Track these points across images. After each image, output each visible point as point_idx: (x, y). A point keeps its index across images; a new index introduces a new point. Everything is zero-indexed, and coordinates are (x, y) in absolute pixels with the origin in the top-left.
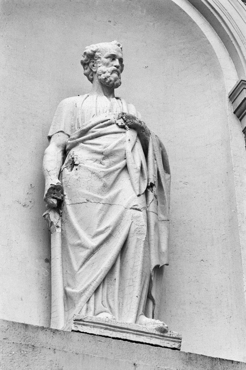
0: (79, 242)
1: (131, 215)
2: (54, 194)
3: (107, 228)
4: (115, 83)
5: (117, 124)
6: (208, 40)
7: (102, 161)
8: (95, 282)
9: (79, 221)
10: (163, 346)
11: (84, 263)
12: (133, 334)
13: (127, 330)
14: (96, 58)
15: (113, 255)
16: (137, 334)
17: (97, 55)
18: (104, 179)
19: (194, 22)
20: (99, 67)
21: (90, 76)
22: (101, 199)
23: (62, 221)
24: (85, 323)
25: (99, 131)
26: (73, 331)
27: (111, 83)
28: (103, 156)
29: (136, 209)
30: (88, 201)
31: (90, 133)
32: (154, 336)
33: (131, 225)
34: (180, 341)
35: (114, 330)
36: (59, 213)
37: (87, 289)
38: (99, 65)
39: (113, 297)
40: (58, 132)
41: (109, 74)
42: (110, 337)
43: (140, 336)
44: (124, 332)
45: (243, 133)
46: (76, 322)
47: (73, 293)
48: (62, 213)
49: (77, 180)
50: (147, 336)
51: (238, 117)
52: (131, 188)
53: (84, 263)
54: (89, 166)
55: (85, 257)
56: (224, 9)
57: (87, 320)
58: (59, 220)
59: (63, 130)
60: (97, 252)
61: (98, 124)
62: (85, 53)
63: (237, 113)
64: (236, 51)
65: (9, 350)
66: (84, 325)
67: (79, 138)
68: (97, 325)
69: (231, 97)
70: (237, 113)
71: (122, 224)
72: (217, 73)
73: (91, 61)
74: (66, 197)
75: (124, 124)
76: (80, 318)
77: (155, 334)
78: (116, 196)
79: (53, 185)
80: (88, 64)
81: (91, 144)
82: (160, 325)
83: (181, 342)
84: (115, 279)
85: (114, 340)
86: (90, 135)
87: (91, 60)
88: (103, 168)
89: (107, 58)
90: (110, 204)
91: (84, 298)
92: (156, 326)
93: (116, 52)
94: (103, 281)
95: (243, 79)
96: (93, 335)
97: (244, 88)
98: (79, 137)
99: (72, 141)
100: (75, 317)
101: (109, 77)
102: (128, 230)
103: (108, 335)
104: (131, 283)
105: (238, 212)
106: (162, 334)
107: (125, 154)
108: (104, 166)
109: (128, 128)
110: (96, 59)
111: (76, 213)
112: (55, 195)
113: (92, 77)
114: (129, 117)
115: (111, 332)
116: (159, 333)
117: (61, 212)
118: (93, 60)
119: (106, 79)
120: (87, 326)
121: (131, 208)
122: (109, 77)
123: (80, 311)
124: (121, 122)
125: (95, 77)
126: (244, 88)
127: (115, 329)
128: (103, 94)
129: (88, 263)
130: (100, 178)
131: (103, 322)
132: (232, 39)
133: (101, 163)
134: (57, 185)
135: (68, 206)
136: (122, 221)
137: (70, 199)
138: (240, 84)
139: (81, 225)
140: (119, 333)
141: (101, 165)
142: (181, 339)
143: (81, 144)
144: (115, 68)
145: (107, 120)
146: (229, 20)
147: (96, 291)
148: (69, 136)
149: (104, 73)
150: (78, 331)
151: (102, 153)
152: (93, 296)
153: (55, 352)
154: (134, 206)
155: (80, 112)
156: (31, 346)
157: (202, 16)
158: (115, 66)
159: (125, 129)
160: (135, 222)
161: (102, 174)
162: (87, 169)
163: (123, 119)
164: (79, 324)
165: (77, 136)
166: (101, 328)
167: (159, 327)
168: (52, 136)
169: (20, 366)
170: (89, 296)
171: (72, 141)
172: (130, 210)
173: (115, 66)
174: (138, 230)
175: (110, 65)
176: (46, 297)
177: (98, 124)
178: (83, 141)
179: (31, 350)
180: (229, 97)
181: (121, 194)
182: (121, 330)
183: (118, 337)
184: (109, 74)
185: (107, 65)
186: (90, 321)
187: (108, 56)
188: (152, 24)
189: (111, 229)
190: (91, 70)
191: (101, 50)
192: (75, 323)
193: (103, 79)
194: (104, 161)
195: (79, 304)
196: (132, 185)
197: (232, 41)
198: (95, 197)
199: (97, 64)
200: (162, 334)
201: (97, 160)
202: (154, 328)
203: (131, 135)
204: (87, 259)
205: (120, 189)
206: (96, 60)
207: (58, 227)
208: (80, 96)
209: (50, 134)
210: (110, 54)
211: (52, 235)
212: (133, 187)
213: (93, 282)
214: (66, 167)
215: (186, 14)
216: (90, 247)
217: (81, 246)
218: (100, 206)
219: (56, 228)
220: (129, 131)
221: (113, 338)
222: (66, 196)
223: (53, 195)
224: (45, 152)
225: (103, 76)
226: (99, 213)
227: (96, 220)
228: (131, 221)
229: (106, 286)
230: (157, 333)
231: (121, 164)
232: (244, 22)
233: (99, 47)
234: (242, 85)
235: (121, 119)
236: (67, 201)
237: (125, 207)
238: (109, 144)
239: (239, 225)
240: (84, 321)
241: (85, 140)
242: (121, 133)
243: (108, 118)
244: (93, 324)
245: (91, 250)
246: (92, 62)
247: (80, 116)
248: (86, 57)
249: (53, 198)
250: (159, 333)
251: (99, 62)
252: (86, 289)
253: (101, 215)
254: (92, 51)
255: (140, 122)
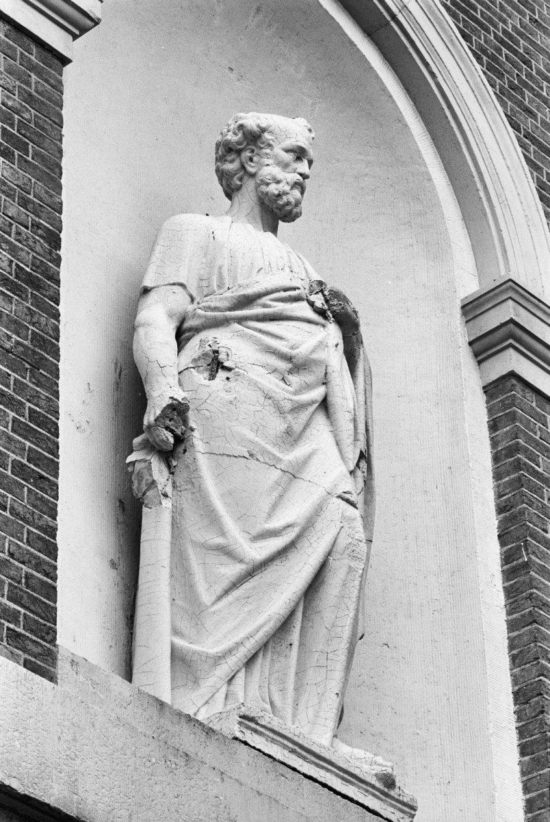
0: (219, 540)
1: (340, 511)
2: (170, 421)
3: (289, 526)
4: (295, 210)
5: (312, 304)
6: (428, 173)
7: (286, 375)
8: (252, 641)
9: (222, 496)
10: (385, 816)
11: (226, 592)
12: (337, 775)
13: (329, 764)
14: (263, 143)
15: (295, 589)
16: (343, 779)
17: (267, 139)
18: (289, 417)
19: (406, 126)
20: (268, 165)
21: (235, 178)
22: (279, 460)
23: (174, 486)
24: (258, 728)
25: (280, 308)
26: (236, 739)
27: (288, 208)
28: (290, 366)
29: (348, 501)
30: (251, 455)
31: (257, 305)
32: (371, 790)
33: (339, 533)
34: (413, 812)
35: (305, 758)
36: (169, 466)
37: (234, 652)
38: (267, 161)
39: (283, 682)
40: (174, 284)
41: (287, 188)
42: (299, 772)
43: (347, 784)
44: (323, 768)
45: (482, 391)
46: (243, 720)
47: (200, 654)
48: (175, 467)
49: (231, 402)
50: (359, 787)
51: (476, 355)
52: (336, 451)
53: (226, 592)
54: (259, 380)
55: (233, 579)
56: (471, 117)
57: (263, 723)
58: (167, 480)
59: (185, 283)
60: (260, 576)
61: (277, 290)
62: (241, 127)
63: (477, 346)
64: (485, 215)
65: (145, 751)
66: (256, 731)
67: (230, 311)
68: (278, 738)
69: (467, 308)
70: (477, 346)
71: (318, 526)
72: (438, 250)
73: (250, 147)
74: (196, 434)
75: (326, 307)
76: (252, 715)
77: (373, 787)
78: (309, 457)
79: (176, 400)
80: (239, 152)
81: (260, 331)
82: (386, 768)
83: (413, 816)
84: (291, 645)
85: (306, 781)
86: (256, 310)
87: (248, 144)
88: (287, 391)
89: (287, 151)
90: (293, 474)
91: (224, 669)
92: (378, 769)
93: (307, 143)
94: (264, 646)
95: (512, 278)
96: (272, 760)
97: (511, 298)
98: (230, 309)
99: (210, 314)
100: (243, 710)
101: (288, 194)
102: (332, 541)
103: (296, 767)
104: (323, 662)
105: (478, 559)
106: (386, 790)
107: (326, 373)
108: (290, 388)
109: (333, 319)
110: (262, 146)
111: (219, 476)
112: (172, 422)
113: (239, 183)
114: (336, 294)
115: (301, 761)
116: (382, 787)
117: (174, 463)
118: (254, 148)
119: (279, 196)
120: (260, 735)
121: (339, 497)
122: (288, 194)
123: (211, 698)
124: (319, 301)
125: (249, 185)
126: (511, 298)
127: (309, 756)
128: (260, 225)
129: (236, 593)
130: (281, 412)
131: (290, 736)
132: (479, 186)
133: (283, 379)
134: (182, 402)
135: (200, 457)
136: (319, 519)
137: (205, 440)
138: (504, 286)
139: (227, 505)
140: (312, 766)
141: (282, 384)
142: (415, 810)
143: (236, 326)
144: (301, 178)
145: (294, 289)
146: (477, 144)
147: (250, 662)
148: (192, 299)
149: (278, 182)
150: (246, 743)
151: (288, 358)
152: (243, 670)
153: (223, 780)
154: (345, 493)
155: (226, 252)
156: (182, 754)
157: (419, 117)
158: (301, 175)
159: (326, 318)
160: (346, 526)
161: (288, 406)
162: (256, 385)
163: (324, 296)
164: (248, 728)
165: (227, 304)
166: (285, 747)
167: (385, 772)
168: (152, 288)
169: (164, 795)
170: (236, 668)
171: (210, 314)
172: (337, 499)
173: (301, 175)
174: (352, 548)
175: (290, 169)
176: (111, 646)
177: (277, 290)
178: (240, 320)
179: (183, 764)
180: (463, 307)
181: (315, 459)
182: (317, 761)
183: (312, 775)
184: (287, 188)
185: (285, 166)
186: (269, 726)
187: (290, 147)
188: (310, 101)
189: (297, 530)
190: (243, 167)
191: (277, 131)
192: (240, 723)
193: (274, 195)
194: (290, 378)
195: (210, 679)
196: (337, 444)
197: (478, 190)
198: (269, 453)
199: (262, 157)
200: (386, 790)
201: (275, 370)
202: (374, 772)
203: (333, 333)
204: (235, 585)
205: (314, 446)
206: (262, 148)
207: (166, 495)
208: (210, 217)
209: (148, 283)
210: (296, 144)
211: (145, 509)
212: (340, 451)
213: (248, 638)
214: (194, 368)
215: (394, 102)
216: (247, 560)
217: (227, 552)
218: (275, 474)
219: (162, 497)
220: (333, 324)
221: (305, 776)
222: (196, 431)
223: (168, 422)
224: (136, 323)
225: (273, 189)
226: (272, 489)
227: (265, 505)
228: (339, 525)
229: (269, 655)
230: (378, 785)
231: (317, 393)
232: (501, 156)
233: (271, 122)
234: (507, 289)
235: (320, 293)
236: (198, 440)
237: (329, 491)
238: (300, 343)
239: (481, 590)
240: (257, 724)
241: (247, 318)
242: (317, 324)
243: (294, 284)
244: (271, 735)
245: (250, 566)
246: (248, 151)
247: (226, 263)
248: (240, 135)
249: (167, 428)
250: (382, 787)
251: (267, 154)
252: (230, 651)
253: (275, 494)
254: (258, 126)
255: (355, 312)
